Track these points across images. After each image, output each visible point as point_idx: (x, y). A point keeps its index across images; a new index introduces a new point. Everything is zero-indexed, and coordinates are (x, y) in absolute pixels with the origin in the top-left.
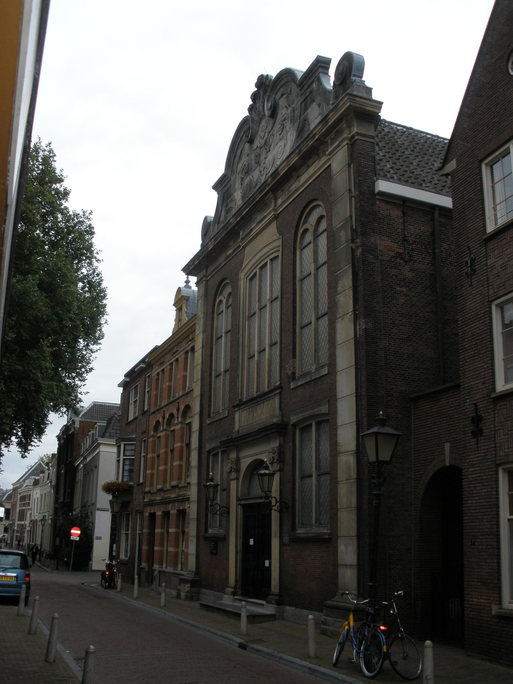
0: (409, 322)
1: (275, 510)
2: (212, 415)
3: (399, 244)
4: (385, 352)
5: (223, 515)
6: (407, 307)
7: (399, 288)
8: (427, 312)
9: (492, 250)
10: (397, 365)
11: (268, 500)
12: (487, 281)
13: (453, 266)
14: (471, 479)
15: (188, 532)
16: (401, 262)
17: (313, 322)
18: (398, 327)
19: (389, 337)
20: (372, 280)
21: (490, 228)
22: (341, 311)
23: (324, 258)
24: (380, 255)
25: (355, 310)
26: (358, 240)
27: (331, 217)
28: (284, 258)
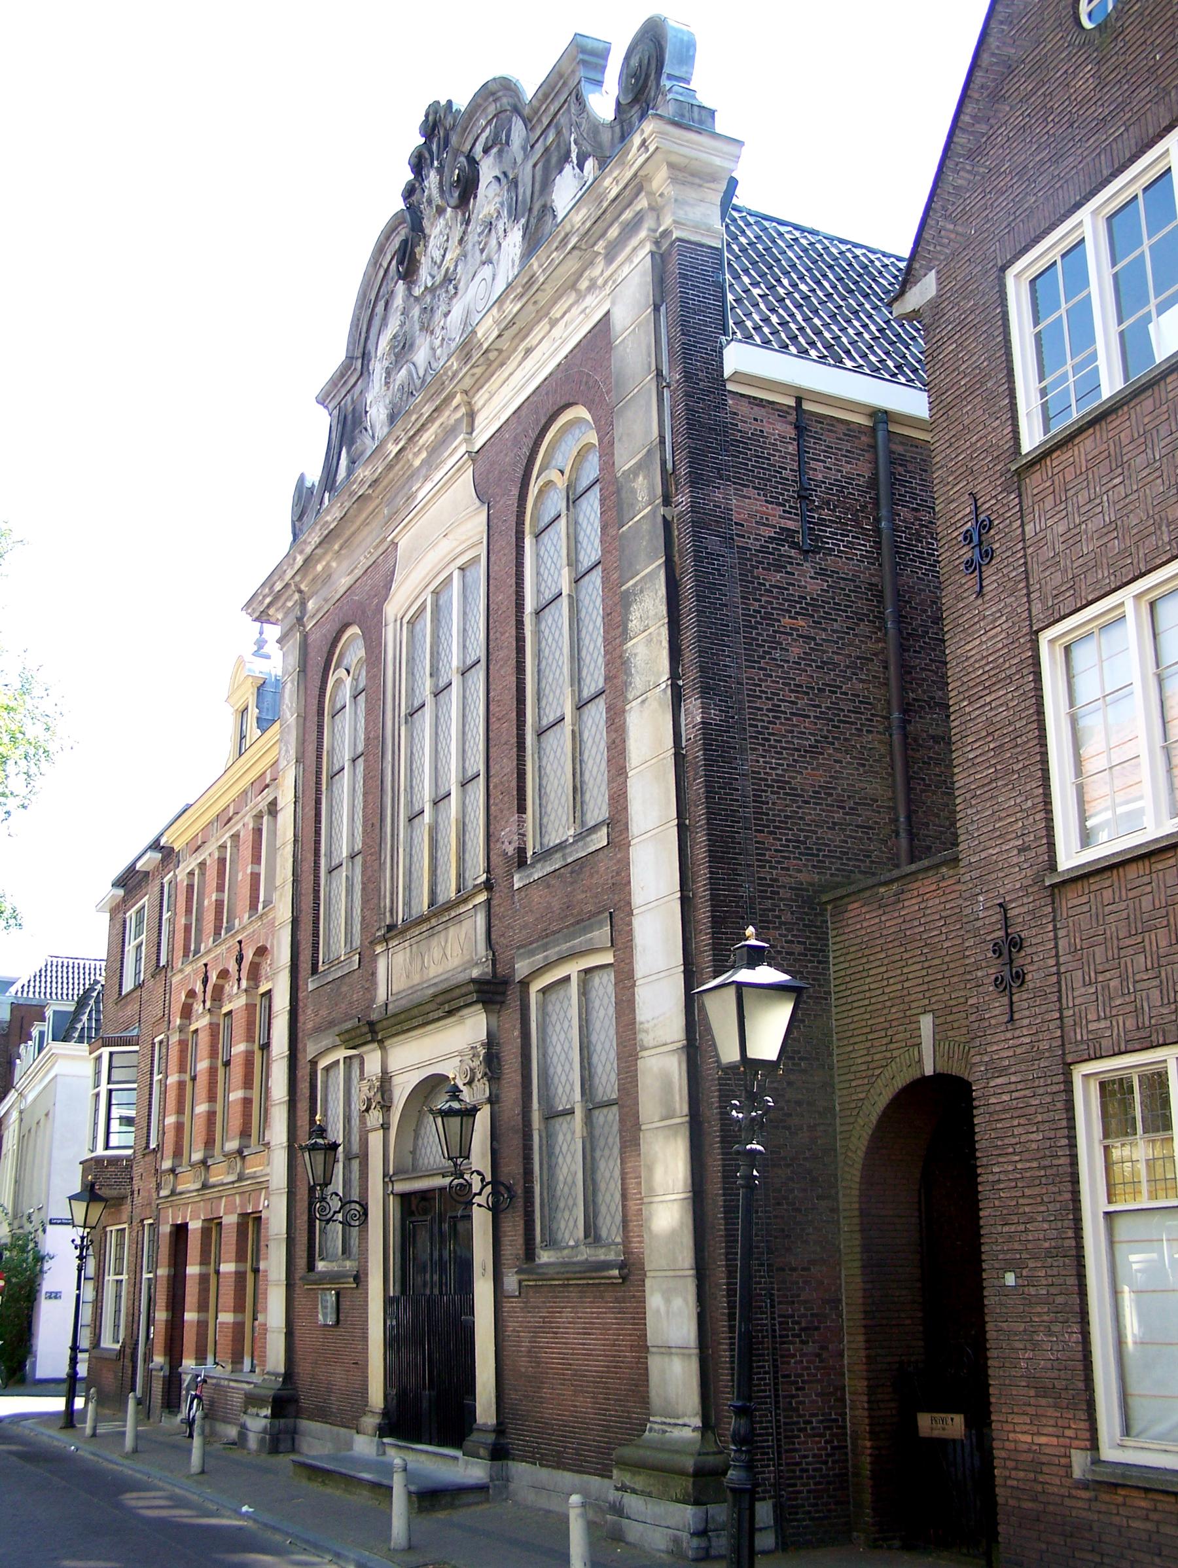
0: (814, 706)
1: (479, 1205)
2: (321, 969)
3: (787, 508)
4: (753, 784)
5: (353, 1223)
6: (808, 669)
7: (787, 620)
8: (862, 681)
9: (1037, 498)
10: (786, 817)
11: (461, 1181)
12: (1027, 578)
13: (925, 564)
14: (998, 1108)
15: (266, 1271)
16: (793, 553)
17: (568, 719)
18: (786, 719)
19: (764, 745)
20: (718, 599)
21: (1031, 438)
22: (638, 682)
23: (594, 553)
24: (738, 535)
25: (674, 676)
26: (679, 498)
27: (612, 444)
28: (492, 559)
